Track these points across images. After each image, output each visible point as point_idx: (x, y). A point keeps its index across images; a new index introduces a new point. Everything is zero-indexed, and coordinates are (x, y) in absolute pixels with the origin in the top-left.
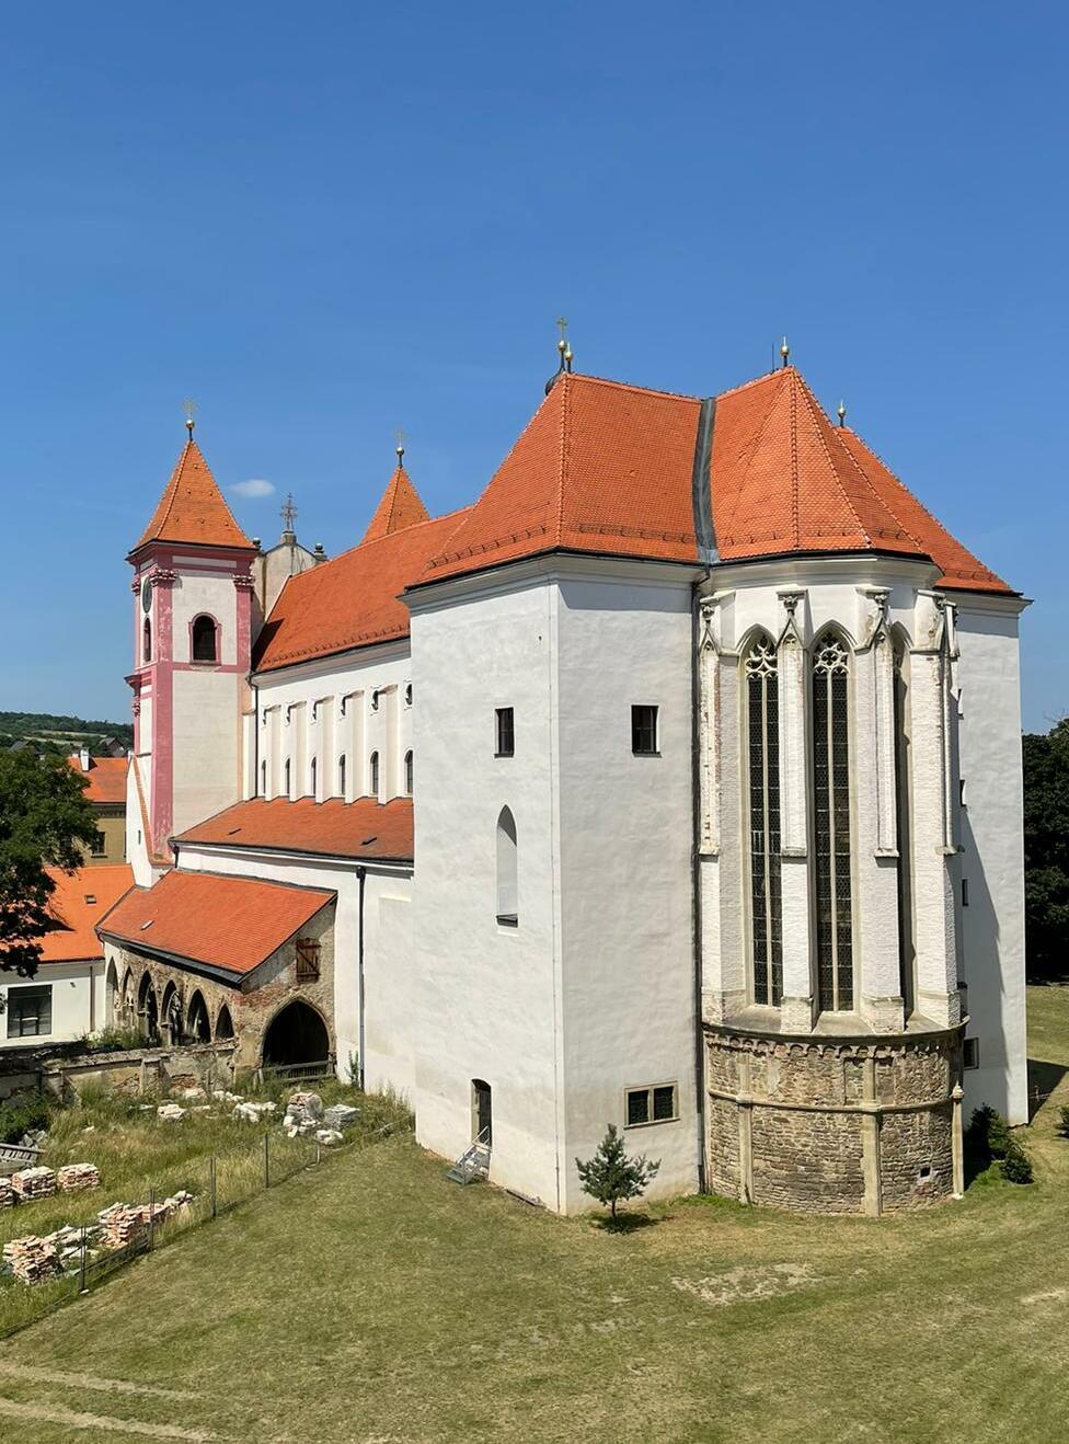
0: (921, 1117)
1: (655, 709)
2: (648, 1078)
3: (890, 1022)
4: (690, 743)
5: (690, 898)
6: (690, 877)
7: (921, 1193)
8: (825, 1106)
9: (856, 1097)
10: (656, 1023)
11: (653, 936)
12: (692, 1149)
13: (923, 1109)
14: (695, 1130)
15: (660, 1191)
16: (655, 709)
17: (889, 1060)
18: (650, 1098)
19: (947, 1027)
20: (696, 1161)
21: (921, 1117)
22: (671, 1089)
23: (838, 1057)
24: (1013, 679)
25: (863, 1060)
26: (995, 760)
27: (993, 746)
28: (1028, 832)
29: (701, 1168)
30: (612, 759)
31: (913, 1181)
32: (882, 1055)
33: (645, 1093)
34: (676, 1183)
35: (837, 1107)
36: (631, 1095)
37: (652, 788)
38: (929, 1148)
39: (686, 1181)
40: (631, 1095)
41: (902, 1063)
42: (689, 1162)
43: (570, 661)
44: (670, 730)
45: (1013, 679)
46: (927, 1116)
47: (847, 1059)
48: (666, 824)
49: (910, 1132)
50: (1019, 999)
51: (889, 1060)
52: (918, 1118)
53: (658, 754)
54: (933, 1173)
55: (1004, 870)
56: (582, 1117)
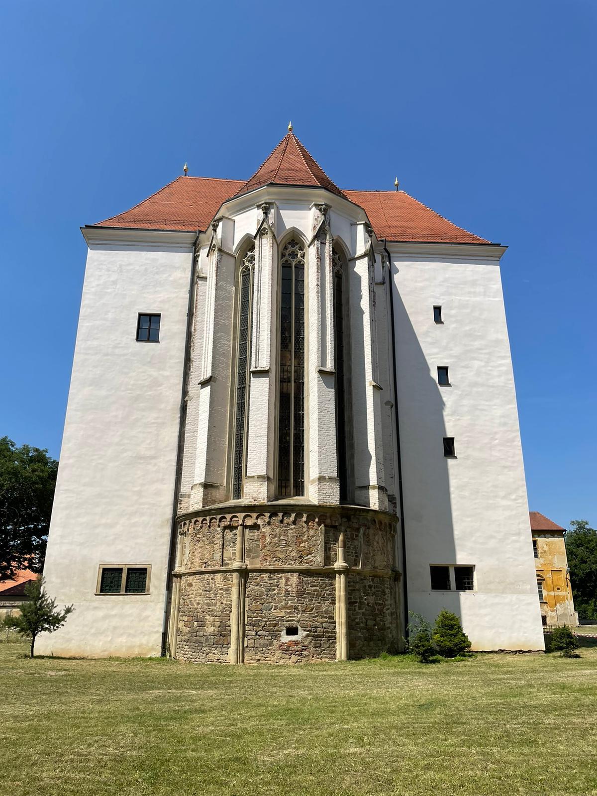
0: (287, 580)
1: (159, 316)
2: (124, 557)
3: (255, 495)
4: (184, 336)
5: (177, 434)
6: (178, 421)
7: (286, 649)
8: (210, 569)
9: (230, 559)
10: (135, 520)
11: (141, 458)
12: (158, 619)
13: (292, 571)
14: (162, 606)
15: (124, 650)
16: (159, 316)
17: (255, 527)
18: (124, 575)
19: (316, 503)
20: (161, 630)
21: (287, 580)
22: (145, 569)
23: (219, 526)
24: (497, 299)
25: (236, 528)
26: (482, 354)
27: (477, 344)
28: (284, 313)
29: (165, 635)
30: (119, 344)
31: (276, 635)
32: (249, 522)
33: (121, 570)
34: (140, 646)
35: (217, 568)
36: (105, 570)
37: (150, 362)
38: (296, 608)
39: (150, 645)
40: (105, 570)
41: (266, 530)
42: (156, 630)
43: (93, 287)
44: (172, 328)
45: (497, 299)
46: (294, 579)
47: (225, 528)
48: (160, 385)
49: (275, 592)
50: (522, 538)
51: (255, 527)
52: (283, 580)
53: (455, 458)
54: (302, 633)
55: (496, 433)
56: (59, 581)
